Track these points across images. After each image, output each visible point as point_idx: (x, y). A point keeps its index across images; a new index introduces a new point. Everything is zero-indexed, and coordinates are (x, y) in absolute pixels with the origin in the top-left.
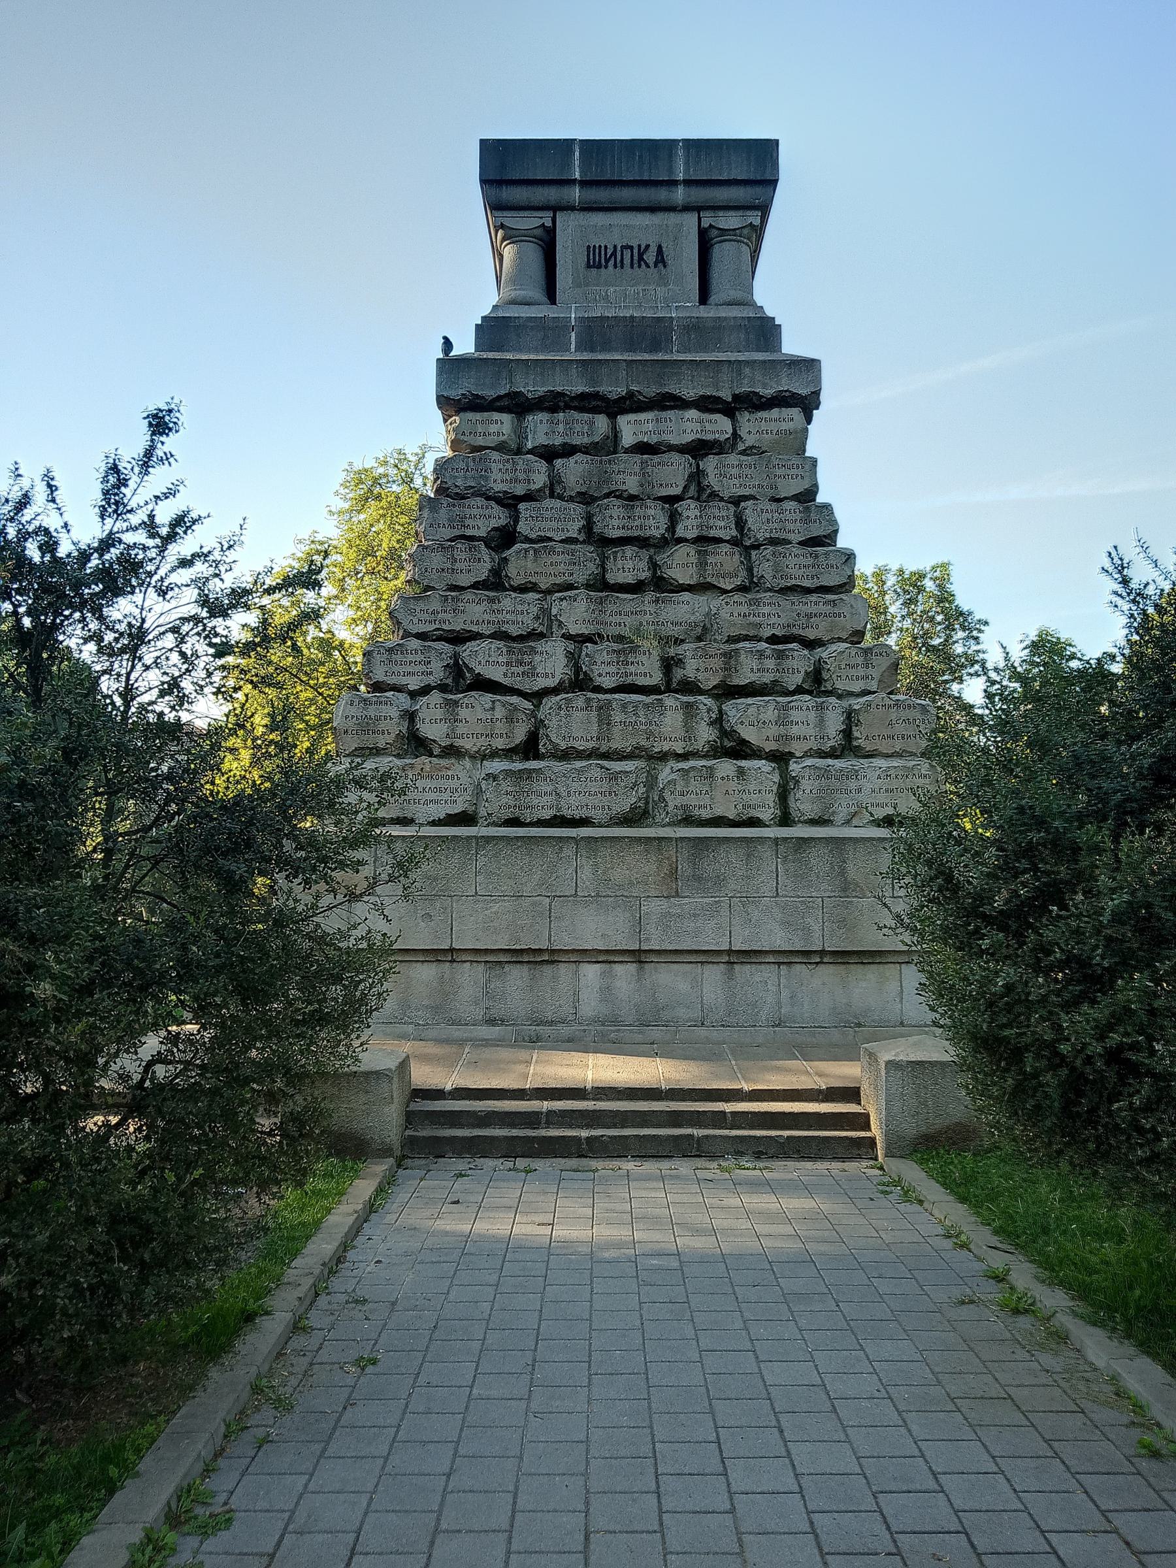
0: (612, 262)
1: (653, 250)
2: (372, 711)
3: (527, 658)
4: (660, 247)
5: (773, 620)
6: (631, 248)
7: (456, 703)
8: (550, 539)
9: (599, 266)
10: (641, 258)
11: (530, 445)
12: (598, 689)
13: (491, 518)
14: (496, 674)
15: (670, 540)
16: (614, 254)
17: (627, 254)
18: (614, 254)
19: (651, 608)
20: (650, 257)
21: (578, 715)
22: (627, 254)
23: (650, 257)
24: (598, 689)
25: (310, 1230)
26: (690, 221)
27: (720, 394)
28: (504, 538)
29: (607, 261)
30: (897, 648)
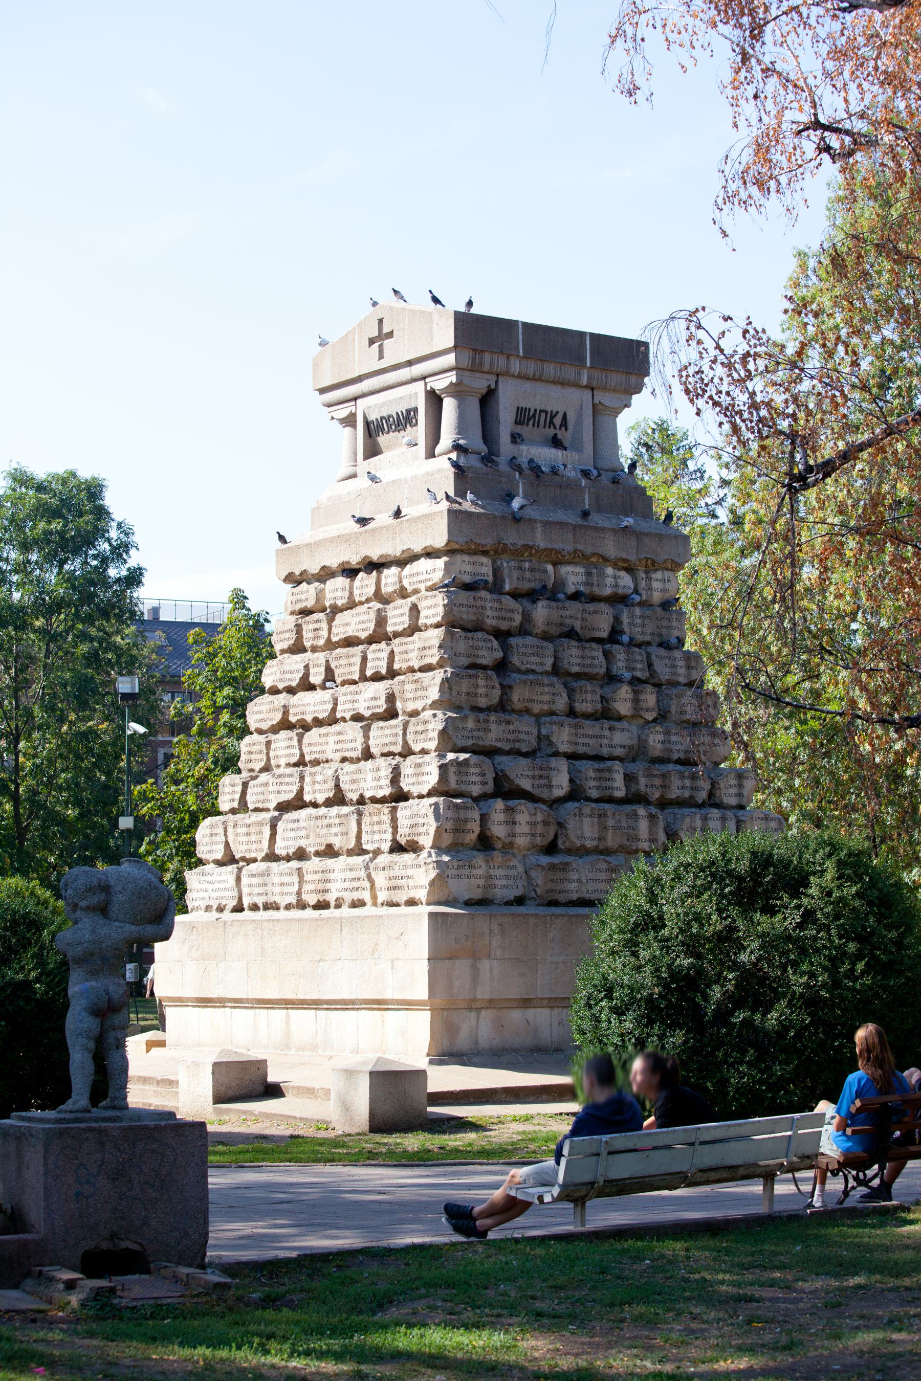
0: (531, 423)
1: (560, 416)
2: (462, 814)
3: (544, 773)
4: (565, 415)
5: (679, 747)
6: (546, 412)
7: (512, 809)
8: (533, 671)
9: (522, 424)
10: (551, 422)
11: (507, 587)
12: (589, 799)
13: (490, 653)
14: (526, 784)
15: (611, 679)
16: (534, 416)
17: (543, 415)
18: (534, 416)
19: (607, 733)
20: (558, 421)
21: (587, 821)
22: (543, 415)
23: (558, 421)
24: (589, 799)
25: (44, 1129)
26: (419, 387)
27: (630, 558)
28: (502, 667)
29: (529, 419)
30: (845, 777)
